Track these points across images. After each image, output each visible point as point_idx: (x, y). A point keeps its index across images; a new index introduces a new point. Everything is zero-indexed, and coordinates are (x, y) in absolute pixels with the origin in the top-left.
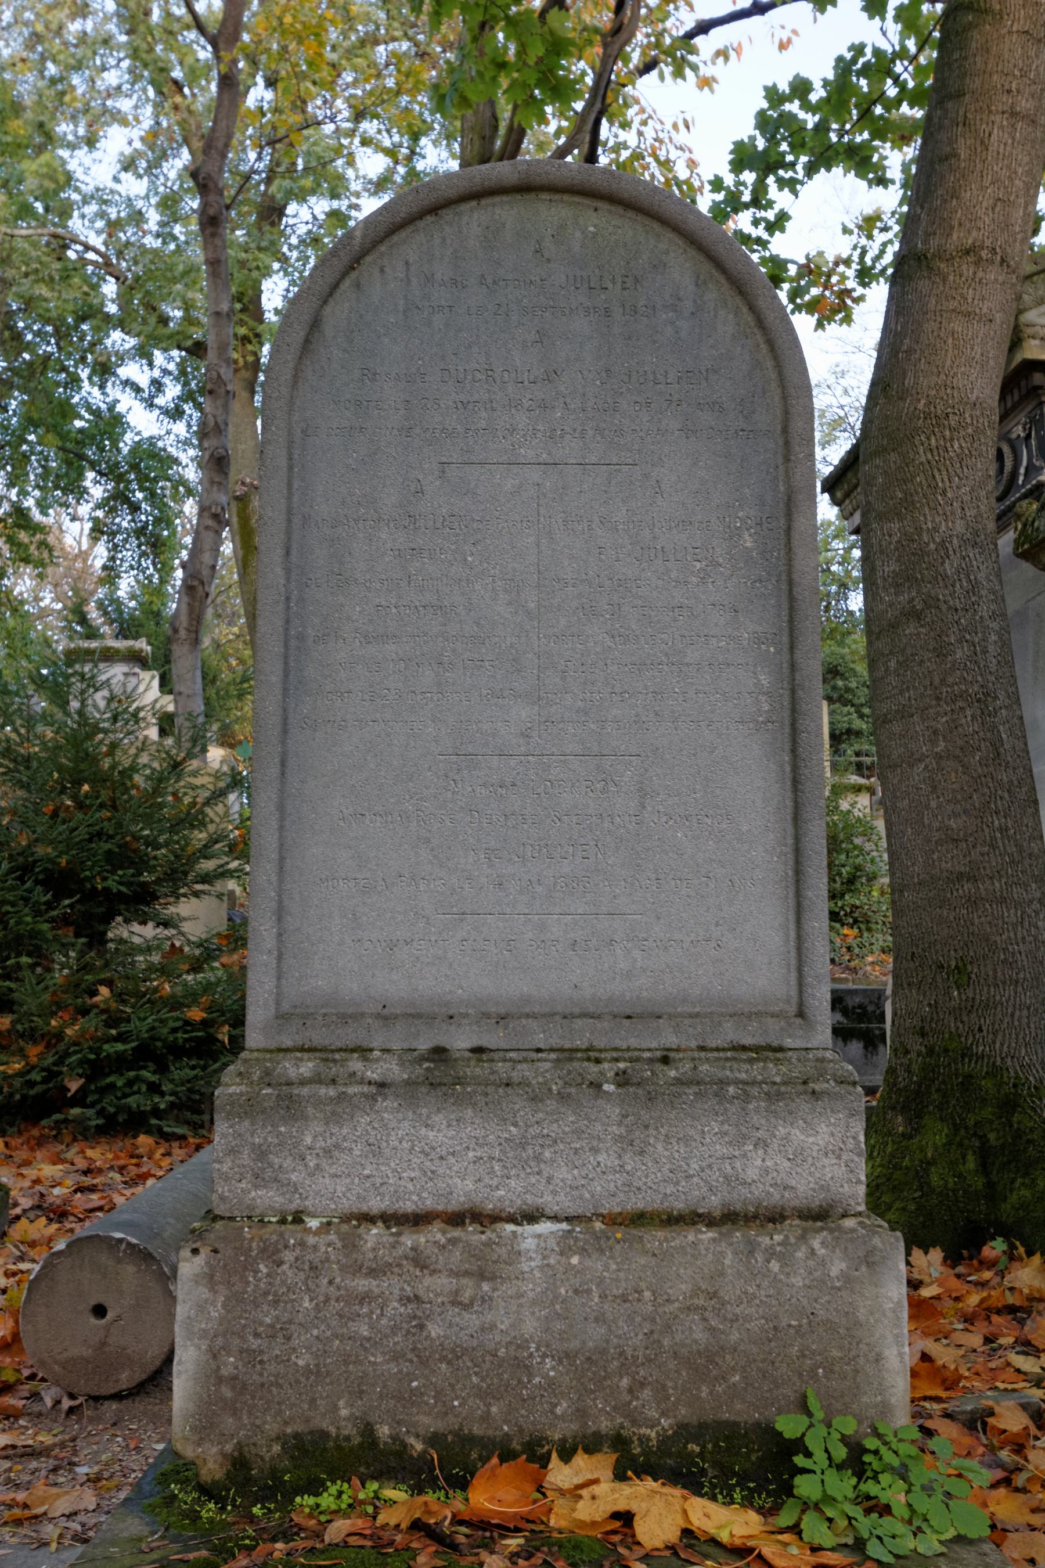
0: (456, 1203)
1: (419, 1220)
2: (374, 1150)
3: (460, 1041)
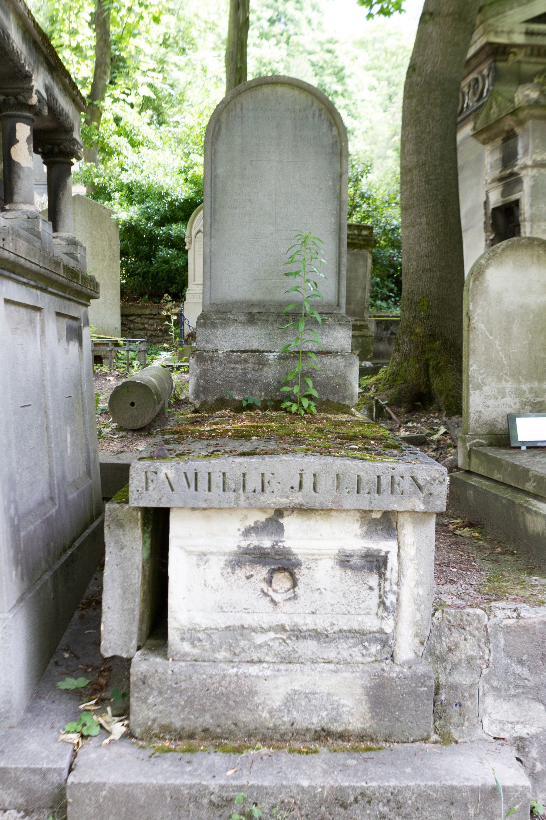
0: (254, 348)
1: (244, 352)
2: (234, 335)
3: (255, 311)
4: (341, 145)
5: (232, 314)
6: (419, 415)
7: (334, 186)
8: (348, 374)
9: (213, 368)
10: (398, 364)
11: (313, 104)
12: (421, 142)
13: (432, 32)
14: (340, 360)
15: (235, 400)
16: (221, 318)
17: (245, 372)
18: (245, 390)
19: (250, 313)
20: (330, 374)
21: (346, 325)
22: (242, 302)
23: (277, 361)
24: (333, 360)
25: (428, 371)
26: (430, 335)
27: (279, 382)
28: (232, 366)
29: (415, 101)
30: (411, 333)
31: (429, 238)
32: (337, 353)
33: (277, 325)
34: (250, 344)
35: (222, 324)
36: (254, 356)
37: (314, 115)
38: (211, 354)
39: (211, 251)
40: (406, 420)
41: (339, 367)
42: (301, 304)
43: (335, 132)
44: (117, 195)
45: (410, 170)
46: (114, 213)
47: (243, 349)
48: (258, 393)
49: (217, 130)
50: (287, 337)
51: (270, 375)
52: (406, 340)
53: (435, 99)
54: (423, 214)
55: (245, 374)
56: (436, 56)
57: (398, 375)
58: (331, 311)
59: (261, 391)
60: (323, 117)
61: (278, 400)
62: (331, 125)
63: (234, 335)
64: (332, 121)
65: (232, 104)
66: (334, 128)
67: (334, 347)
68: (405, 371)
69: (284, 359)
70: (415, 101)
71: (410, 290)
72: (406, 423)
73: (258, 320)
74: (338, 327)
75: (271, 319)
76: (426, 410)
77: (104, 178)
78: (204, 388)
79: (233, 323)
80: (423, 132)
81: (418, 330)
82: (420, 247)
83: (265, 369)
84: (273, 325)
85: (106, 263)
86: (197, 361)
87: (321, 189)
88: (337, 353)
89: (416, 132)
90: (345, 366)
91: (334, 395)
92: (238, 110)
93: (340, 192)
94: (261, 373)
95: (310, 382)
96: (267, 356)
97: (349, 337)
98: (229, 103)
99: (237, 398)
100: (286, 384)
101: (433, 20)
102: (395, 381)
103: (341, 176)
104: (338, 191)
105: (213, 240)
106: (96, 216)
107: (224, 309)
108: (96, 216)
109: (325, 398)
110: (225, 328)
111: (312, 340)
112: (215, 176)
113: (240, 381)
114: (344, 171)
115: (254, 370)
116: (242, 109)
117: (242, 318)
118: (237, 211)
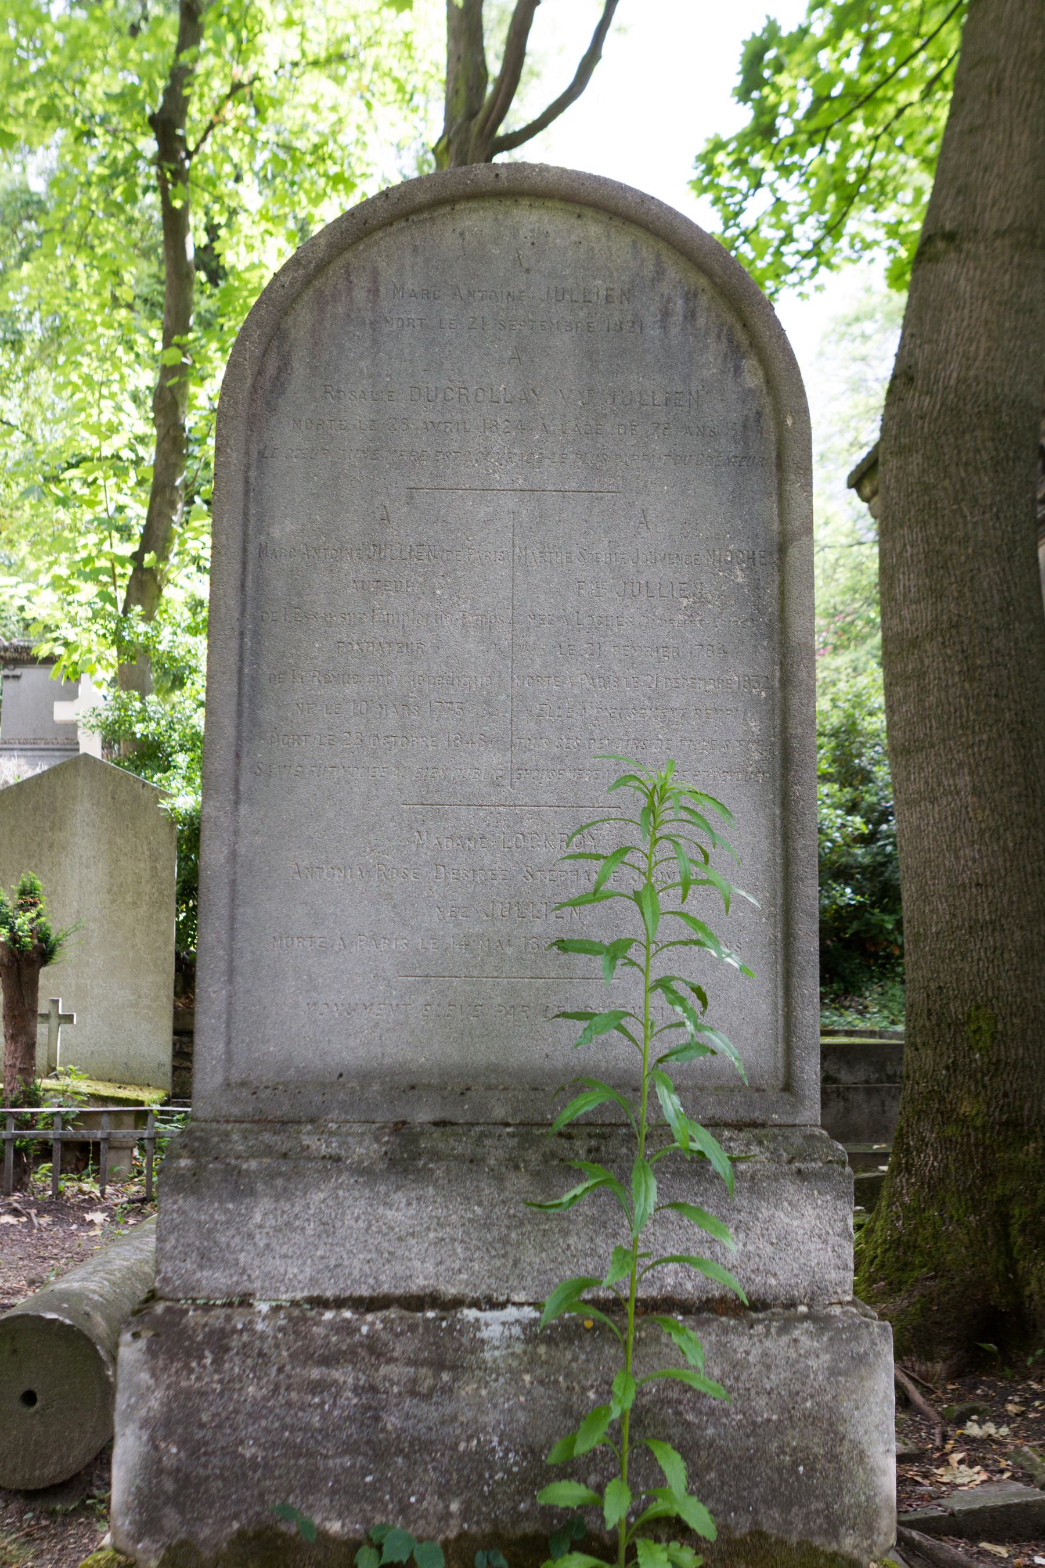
0: (418, 1284)
2: (327, 1228)
3: (423, 1115)
4: (780, 424)
5: (321, 1131)
6: (992, 1386)
7: (756, 587)
8: (846, 1406)
9: (227, 1386)
10: (913, 1212)
11: (660, 273)
12: (945, 567)
13: (957, 280)
14: (807, 1343)
15: (324, 1536)
16: (269, 1151)
17: (372, 1404)
18: (374, 1487)
19: (400, 1127)
20: (765, 1410)
21: (826, 1177)
22: (365, 1077)
23: (519, 1348)
24: (777, 1345)
25: (1008, 1235)
26: (1007, 1124)
27: (532, 1452)
28: (315, 1373)
29: (917, 458)
30: (947, 1116)
31: (982, 833)
32: (792, 1304)
33: (519, 1182)
34: (398, 1268)
35: (272, 1175)
36: (413, 1328)
37: (666, 314)
38: (217, 1318)
39: (233, 856)
40: (957, 1408)
41: (803, 1376)
42: (627, 1085)
43: (752, 378)
44: (181, 759)
45: (914, 643)
46: (165, 795)
47: (365, 1292)
48: (431, 1503)
49: (271, 371)
50: (565, 1233)
51: (491, 1418)
52: (931, 1137)
53: (977, 451)
54: (961, 765)
55: (371, 1414)
56: (971, 340)
57: (912, 1247)
58: (757, 1115)
59: (444, 1492)
60: (701, 321)
61: (526, 1541)
62: (735, 352)
63: (327, 1228)
64: (740, 336)
65: (335, 269)
66: (749, 364)
67: (782, 1277)
68: (936, 1236)
69: (549, 1341)
70: (917, 458)
71: (933, 986)
72: (961, 1420)
73: (435, 1155)
74: (791, 1189)
75: (495, 1154)
76: (1012, 1366)
77: (158, 724)
78: (184, 1480)
79: (325, 1175)
80: (945, 539)
81: (966, 1108)
82: (957, 858)
83: (467, 1389)
84: (499, 1179)
85: (143, 910)
86: (151, 1352)
87: (702, 600)
88: (792, 1304)
89: (927, 541)
90: (833, 1372)
91: (786, 1508)
92: (360, 295)
93: (783, 609)
94: (448, 1410)
95: (674, 1468)
96: (476, 1325)
97: (844, 1234)
98: (321, 268)
99: (335, 1527)
100: (569, 1470)
101: (959, 249)
102: (905, 1267)
103: (782, 550)
104: (773, 608)
105: (244, 810)
106: (124, 803)
107: (285, 1109)
108: (124, 803)
109: (742, 1526)
110: (285, 1194)
111: (673, 1245)
112: (262, 550)
113: (350, 1448)
114: (796, 524)
115: (413, 1393)
116: (374, 292)
117: (365, 1149)
118: (350, 689)
